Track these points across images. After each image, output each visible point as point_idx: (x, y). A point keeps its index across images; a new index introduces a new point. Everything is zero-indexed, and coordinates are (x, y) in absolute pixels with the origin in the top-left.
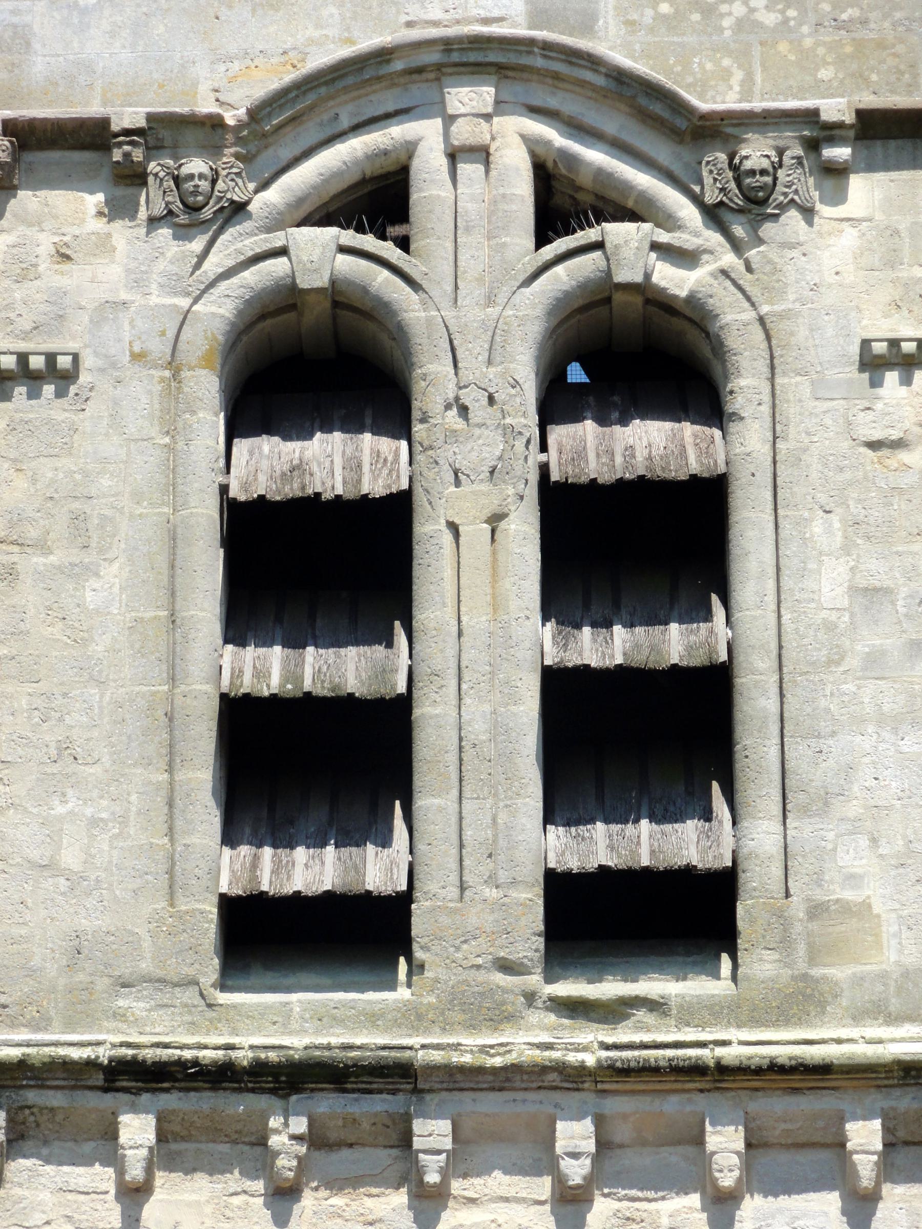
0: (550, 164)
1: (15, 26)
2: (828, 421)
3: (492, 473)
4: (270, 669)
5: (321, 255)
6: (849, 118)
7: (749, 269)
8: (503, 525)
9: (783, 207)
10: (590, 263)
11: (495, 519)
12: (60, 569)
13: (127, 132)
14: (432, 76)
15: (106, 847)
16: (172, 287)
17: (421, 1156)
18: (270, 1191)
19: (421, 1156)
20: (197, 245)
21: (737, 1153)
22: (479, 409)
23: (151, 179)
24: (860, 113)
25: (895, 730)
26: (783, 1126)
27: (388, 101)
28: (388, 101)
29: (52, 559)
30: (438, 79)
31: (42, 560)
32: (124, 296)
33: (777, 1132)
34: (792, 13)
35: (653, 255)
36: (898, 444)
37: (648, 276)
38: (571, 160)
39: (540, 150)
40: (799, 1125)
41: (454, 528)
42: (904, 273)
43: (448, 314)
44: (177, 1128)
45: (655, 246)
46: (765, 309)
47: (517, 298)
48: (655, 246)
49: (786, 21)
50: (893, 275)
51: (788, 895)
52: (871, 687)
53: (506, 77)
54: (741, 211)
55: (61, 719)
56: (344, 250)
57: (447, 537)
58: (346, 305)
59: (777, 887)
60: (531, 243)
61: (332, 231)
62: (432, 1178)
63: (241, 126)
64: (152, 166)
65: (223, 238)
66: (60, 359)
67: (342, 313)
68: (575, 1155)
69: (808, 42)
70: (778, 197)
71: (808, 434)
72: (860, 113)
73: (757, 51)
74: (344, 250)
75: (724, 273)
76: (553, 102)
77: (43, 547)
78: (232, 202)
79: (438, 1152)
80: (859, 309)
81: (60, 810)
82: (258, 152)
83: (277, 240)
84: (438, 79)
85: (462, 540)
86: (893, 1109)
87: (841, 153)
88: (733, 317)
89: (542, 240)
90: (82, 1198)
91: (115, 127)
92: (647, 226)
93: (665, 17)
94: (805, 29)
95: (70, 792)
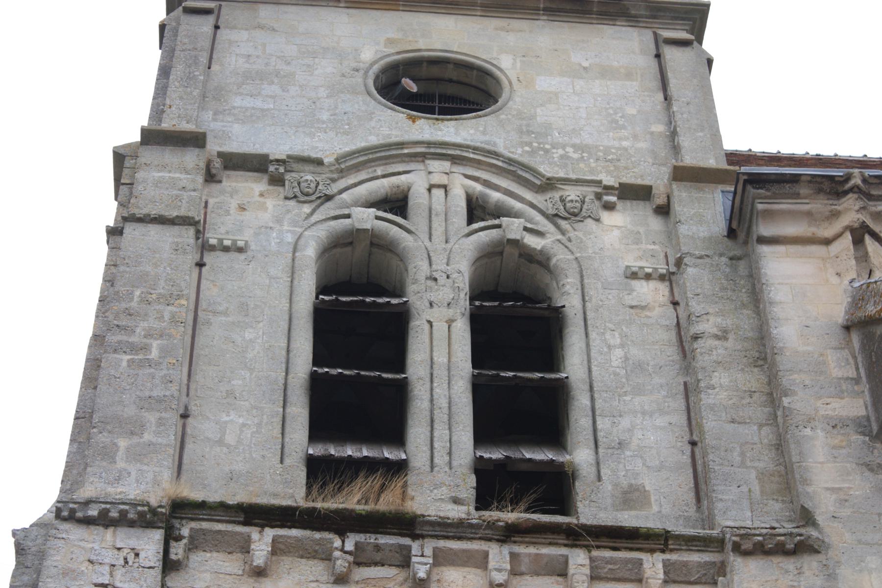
0: (474, 199)
1: (224, 131)
2: (610, 297)
3: (449, 305)
4: (317, 450)
5: (366, 218)
6: (617, 185)
7: (570, 240)
8: (454, 324)
9: (585, 218)
10: (494, 233)
11: (450, 322)
12: (233, 323)
13: (277, 161)
14: (420, 159)
15: (249, 436)
16: (294, 223)
17: (416, 565)
18: (332, 579)
19: (416, 565)
20: (307, 209)
21: (586, 575)
22: (442, 280)
23: (287, 183)
24: (620, 184)
25: (651, 416)
26: (610, 566)
27: (400, 168)
28: (400, 168)
29: (230, 319)
30: (423, 161)
31: (223, 318)
32: (271, 224)
33: (606, 570)
34: (585, 155)
35: (525, 233)
36: (643, 308)
37: (523, 239)
38: (484, 196)
39: (470, 191)
40: (617, 567)
41: (430, 323)
42: (643, 246)
43: (428, 244)
44: (282, 547)
45: (526, 229)
46: (578, 255)
47: (460, 242)
48: (526, 229)
49: (583, 157)
50: (637, 247)
51: (599, 478)
52: (637, 400)
53: (455, 163)
54: (565, 219)
55: (229, 382)
56: (378, 218)
57: (427, 327)
58: (378, 244)
59: (593, 476)
60: (465, 222)
61: (372, 211)
62: (422, 574)
63: (331, 165)
64: (288, 177)
65: (322, 208)
66: (239, 242)
67: (375, 250)
68: (499, 570)
69: (593, 165)
70: (584, 213)
71: (601, 301)
72: (620, 184)
73: (570, 166)
74: (378, 218)
75: (558, 240)
76: (477, 173)
77: (225, 313)
78: (326, 195)
79: (426, 564)
80: (622, 258)
81: (227, 419)
82: (339, 179)
83: (346, 211)
84: (423, 161)
85: (434, 328)
86: (669, 560)
87: (613, 199)
88: (560, 257)
89: (470, 221)
90: (228, 577)
91: (271, 158)
92: (522, 220)
93: (528, 152)
94: (592, 160)
95: (232, 412)
